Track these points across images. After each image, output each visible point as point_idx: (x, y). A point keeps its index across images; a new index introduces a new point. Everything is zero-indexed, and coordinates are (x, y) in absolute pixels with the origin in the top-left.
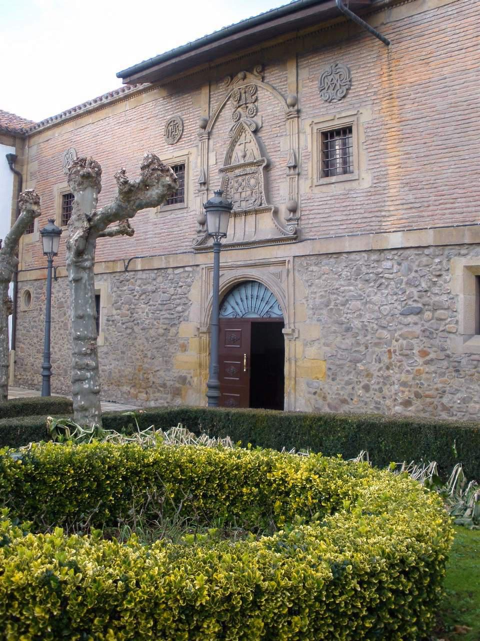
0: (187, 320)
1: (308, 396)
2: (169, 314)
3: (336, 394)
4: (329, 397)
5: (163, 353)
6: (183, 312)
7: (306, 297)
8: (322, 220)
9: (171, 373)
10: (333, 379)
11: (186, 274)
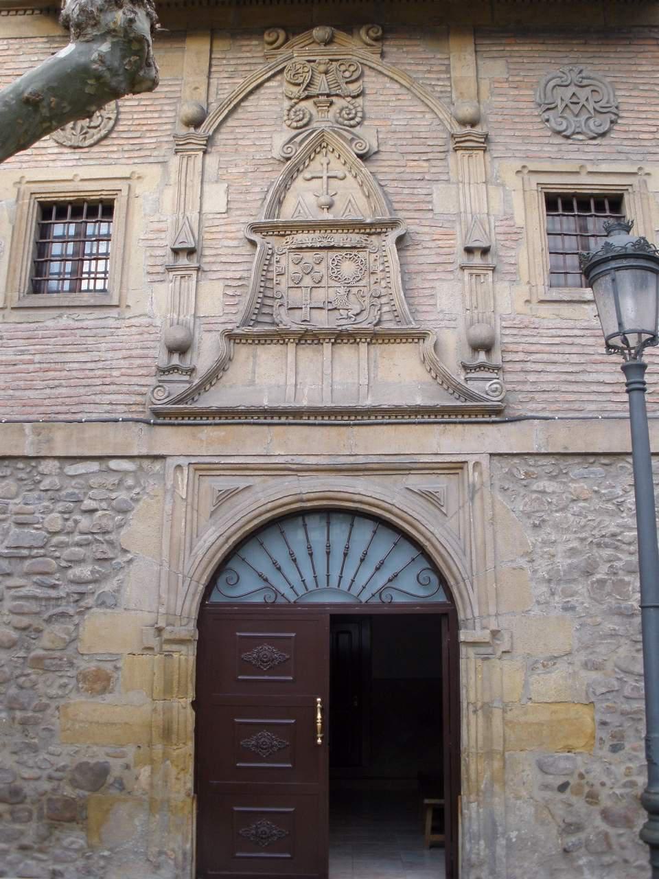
0: (109, 603)
1: (539, 795)
2: (40, 585)
3: (625, 786)
4: (604, 794)
5: (14, 699)
6: (95, 581)
7: (527, 554)
8: (563, 377)
9: (43, 755)
10: (615, 749)
11: (114, 479)
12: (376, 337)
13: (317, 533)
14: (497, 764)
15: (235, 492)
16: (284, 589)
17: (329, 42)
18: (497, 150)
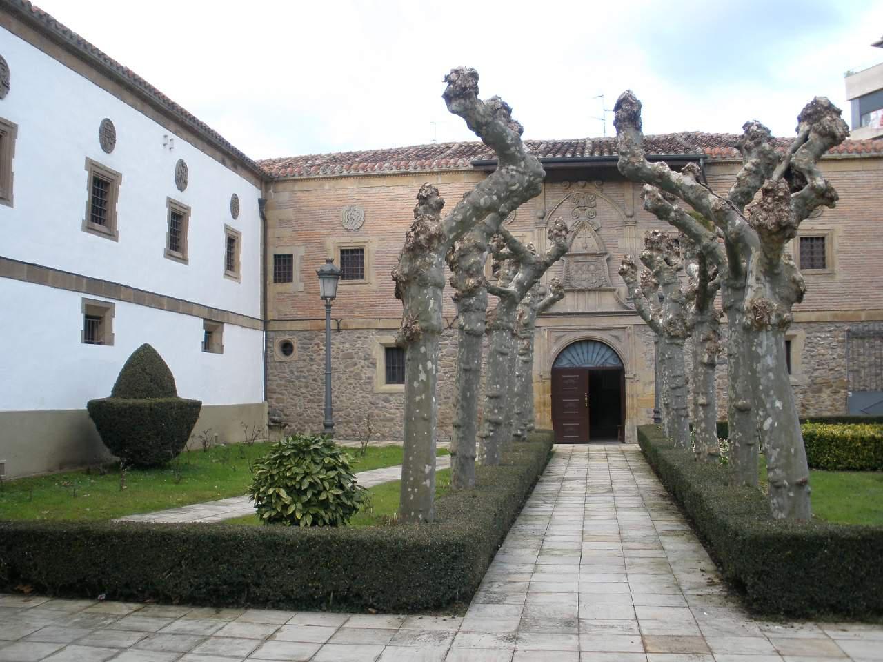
12: (601, 291)
13: (585, 347)
14: (635, 411)
15: (561, 336)
16: (576, 363)
17: (583, 187)
18: (639, 225)
